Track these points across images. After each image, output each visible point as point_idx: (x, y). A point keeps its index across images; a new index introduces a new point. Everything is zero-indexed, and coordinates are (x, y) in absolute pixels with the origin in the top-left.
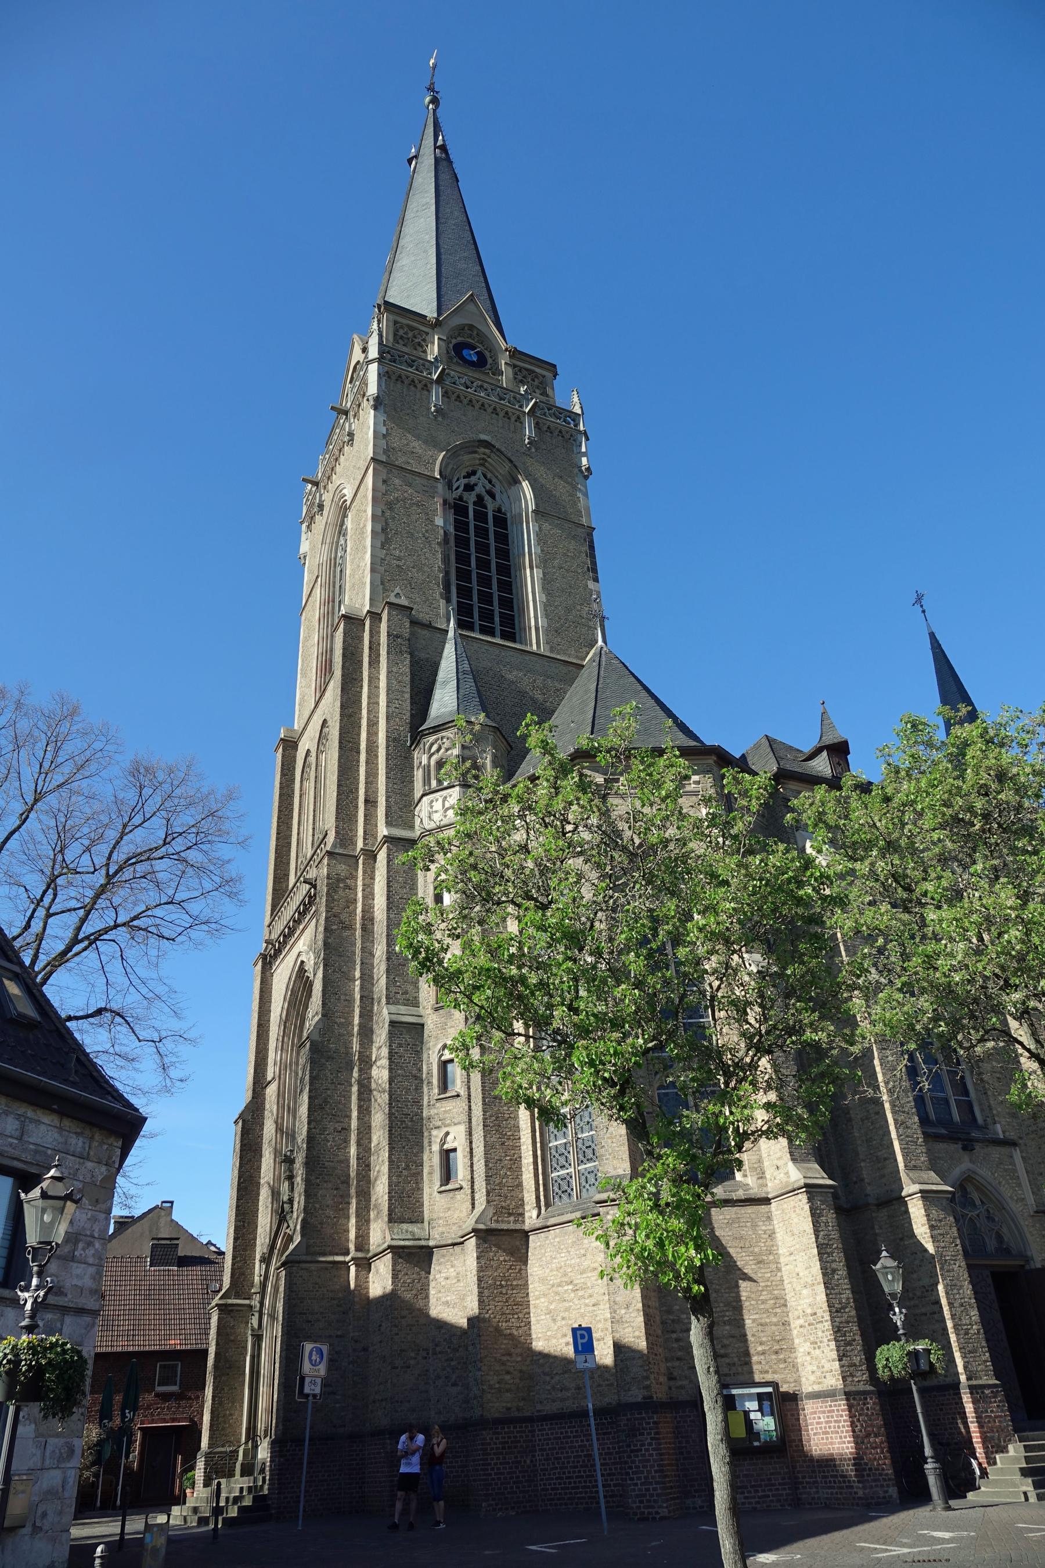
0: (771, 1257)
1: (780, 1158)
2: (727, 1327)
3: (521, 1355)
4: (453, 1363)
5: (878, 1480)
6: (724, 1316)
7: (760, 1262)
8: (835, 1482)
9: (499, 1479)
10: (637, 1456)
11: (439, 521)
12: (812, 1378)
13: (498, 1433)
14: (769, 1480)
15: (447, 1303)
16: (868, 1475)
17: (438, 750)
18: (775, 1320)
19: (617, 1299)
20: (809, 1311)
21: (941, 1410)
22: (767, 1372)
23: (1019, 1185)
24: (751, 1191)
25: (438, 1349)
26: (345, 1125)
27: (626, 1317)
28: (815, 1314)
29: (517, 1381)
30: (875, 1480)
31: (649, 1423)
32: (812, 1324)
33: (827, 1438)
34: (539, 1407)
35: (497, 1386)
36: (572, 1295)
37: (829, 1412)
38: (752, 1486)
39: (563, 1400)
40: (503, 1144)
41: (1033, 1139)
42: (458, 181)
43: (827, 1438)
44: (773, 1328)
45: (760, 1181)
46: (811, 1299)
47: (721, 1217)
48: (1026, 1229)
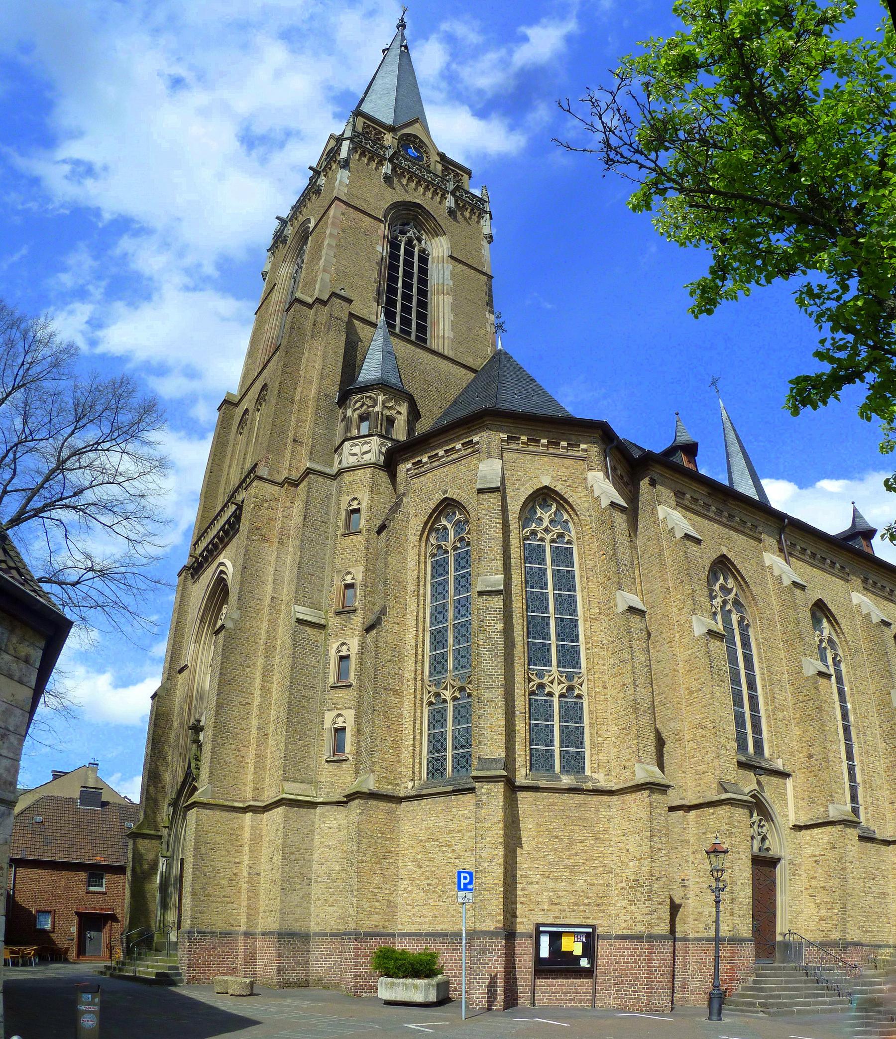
0: (607, 836)
1: (629, 760)
2: (564, 884)
3: (389, 889)
4: (330, 890)
6: (562, 875)
7: (597, 839)
8: (626, 995)
9: (366, 972)
10: (485, 967)
12: (624, 925)
13: (367, 942)
14: (576, 989)
15: (329, 847)
18: (602, 882)
19: (482, 854)
20: (632, 878)
22: (589, 918)
23: (786, 805)
24: (598, 784)
25: (319, 879)
26: (249, 701)
27: (489, 869)
28: (638, 880)
30: (659, 996)
32: (634, 887)
34: (400, 927)
36: (438, 849)
39: (421, 924)
40: (388, 727)
41: (804, 773)
44: (599, 887)
47: (571, 802)
48: (784, 837)
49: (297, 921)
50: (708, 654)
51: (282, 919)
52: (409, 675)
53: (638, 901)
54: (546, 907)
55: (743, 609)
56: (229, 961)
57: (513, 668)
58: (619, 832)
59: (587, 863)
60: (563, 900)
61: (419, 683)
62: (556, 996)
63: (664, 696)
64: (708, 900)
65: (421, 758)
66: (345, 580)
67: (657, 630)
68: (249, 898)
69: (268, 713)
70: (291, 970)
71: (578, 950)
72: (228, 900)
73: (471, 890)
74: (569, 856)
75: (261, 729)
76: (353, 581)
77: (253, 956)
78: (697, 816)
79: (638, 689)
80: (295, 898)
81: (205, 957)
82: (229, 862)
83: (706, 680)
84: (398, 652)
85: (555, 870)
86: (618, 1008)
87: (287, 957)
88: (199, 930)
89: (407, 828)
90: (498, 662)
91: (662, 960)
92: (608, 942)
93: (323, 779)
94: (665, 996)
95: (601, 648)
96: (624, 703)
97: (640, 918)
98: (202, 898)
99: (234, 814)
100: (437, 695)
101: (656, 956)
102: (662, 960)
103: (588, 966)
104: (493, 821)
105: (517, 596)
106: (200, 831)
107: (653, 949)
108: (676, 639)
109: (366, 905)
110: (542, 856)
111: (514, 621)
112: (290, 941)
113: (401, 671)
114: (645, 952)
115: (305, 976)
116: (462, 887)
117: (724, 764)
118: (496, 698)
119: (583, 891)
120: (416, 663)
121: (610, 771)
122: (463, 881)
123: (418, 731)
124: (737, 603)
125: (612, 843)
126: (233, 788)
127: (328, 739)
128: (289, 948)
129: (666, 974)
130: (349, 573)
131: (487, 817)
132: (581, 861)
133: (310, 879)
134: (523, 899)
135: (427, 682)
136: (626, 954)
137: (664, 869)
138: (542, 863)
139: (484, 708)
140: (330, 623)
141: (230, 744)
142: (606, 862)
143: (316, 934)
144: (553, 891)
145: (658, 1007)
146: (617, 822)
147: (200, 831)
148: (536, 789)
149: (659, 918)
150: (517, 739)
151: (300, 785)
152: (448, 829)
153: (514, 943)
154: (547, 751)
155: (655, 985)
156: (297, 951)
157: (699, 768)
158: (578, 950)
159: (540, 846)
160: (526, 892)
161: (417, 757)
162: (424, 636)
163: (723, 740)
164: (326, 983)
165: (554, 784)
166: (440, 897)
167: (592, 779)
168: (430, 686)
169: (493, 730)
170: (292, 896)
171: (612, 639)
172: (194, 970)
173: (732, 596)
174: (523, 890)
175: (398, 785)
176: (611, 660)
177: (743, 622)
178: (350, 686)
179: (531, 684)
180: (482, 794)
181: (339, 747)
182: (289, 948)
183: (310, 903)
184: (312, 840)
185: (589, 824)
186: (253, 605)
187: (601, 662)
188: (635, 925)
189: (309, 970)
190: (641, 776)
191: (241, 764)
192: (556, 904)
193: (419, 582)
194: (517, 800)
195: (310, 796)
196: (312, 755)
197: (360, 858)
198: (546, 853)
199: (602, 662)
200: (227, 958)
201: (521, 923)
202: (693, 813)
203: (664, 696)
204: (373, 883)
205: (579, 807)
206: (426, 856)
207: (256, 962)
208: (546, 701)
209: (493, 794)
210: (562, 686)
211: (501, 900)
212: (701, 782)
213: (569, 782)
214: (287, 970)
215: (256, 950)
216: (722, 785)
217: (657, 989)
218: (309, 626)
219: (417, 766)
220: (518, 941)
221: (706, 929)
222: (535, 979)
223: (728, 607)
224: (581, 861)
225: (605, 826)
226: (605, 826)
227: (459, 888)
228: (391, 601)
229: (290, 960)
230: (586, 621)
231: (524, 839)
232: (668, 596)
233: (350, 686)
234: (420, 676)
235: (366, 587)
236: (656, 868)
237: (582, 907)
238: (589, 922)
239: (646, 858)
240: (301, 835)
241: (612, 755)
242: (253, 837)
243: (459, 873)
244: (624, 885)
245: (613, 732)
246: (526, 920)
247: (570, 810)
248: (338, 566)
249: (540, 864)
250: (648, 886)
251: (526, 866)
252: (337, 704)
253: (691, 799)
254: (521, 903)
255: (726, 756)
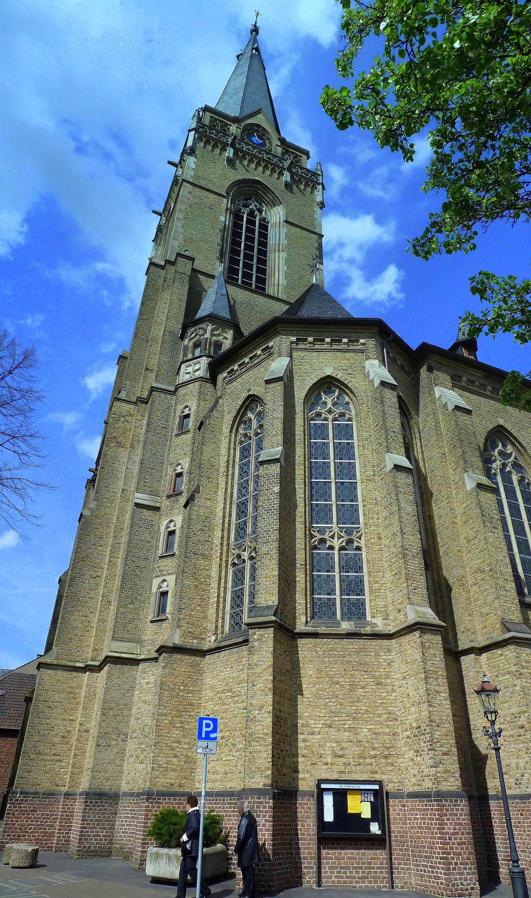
0: (389, 681)
1: (400, 604)
2: (347, 734)
3: (189, 744)
4: (142, 746)
5: (462, 874)
7: (378, 684)
11: (222, 219)
12: (413, 780)
13: (159, 803)
14: (370, 863)
15: (145, 702)
16: (454, 869)
17: (195, 336)
18: (387, 730)
19: (253, 702)
20: (415, 725)
21: (522, 814)
22: (376, 772)
24: (377, 629)
25: (134, 735)
26: (99, 574)
27: (258, 718)
28: (420, 727)
29: (183, 763)
31: (265, 807)
32: (417, 736)
33: (421, 833)
35: (165, 765)
36: (230, 700)
37: (424, 810)
38: (354, 868)
39: (214, 781)
42: (265, 69)
43: (421, 833)
44: (385, 737)
45: (385, 621)
46: (417, 715)
47: (351, 647)
49: (108, 779)
50: (479, 504)
51: (93, 778)
52: (217, 541)
53: (422, 751)
54: (329, 760)
55: (523, 470)
56: (48, 826)
57: (295, 526)
58: (400, 676)
59: (370, 710)
60: (347, 752)
61: (225, 547)
62: (346, 873)
63: (447, 546)
64: (513, 750)
65: (224, 613)
66: (176, 470)
67: (437, 490)
68: (76, 755)
69: (112, 584)
70: (94, 836)
71: (366, 812)
72: (57, 758)
73: (215, 739)
74: (351, 702)
75: (105, 597)
76: (182, 470)
77: (69, 819)
78: (488, 659)
79: (406, 536)
80: (109, 755)
81: (23, 821)
82: (64, 720)
83: (479, 527)
84: (209, 522)
85: (337, 719)
86: (420, 890)
87: (91, 820)
88: (23, 790)
89: (208, 680)
90: (274, 520)
91: (456, 824)
92: (400, 802)
93: (146, 638)
94: (468, 874)
95: (376, 504)
96: (395, 550)
97: (426, 771)
98: (32, 756)
99: (75, 674)
100: (239, 556)
101: (448, 819)
102: (456, 824)
103: (379, 832)
104: (264, 666)
105: (299, 466)
106: (40, 690)
107: (442, 810)
108: (453, 496)
109: (162, 760)
110: (323, 703)
111: (297, 486)
112: (96, 803)
113: (211, 539)
114: (435, 815)
115: (108, 844)
116: (203, 736)
117: (505, 604)
118: (272, 551)
119: (368, 742)
120: (223, 530)
121: (387, 616)
122: (204, 729)
123: (222, 589)
124: (516, 465)
125: (394, 688)
126: (77, 650)
127: (153, 602)
128: (95, 810)
129: (464, 843)
130: (179, 464)
131: (259, 663)
132: (364, 708)
133: (126, 735)
134: (305, 751)
135: (232, 546)
136: (418, 816)
137: (445, 714)
138: (323, 711)
139: (261, 560)
140: (163, 505)
141: (79, 611)
142: (390, 708)
143: (125, 794)
144: (336, 742)
145: (462, 890)
146: (397, 666)
147: (40, 690)
148: (315, 635)
149: (446, 771)
150: (298, 589)
151: (127, 644)
152: (239, 679)
153: (295, 804)
154: (329, 599)
155: (453, 858)
156: (103, 814)
157: (483, 610)
158: (366, 812)
159: (321, 693)
160: (307, 744)
161: (221, 613)
162: (231, 507)
163: (501, 582)
164: (127, 852)
165: (333, 630)
166: (231, 751)
167: (374, 625)
168: (234, 549)
169: (268, 579)
170: (106, 753)
171: (383, 496)
172: (8, 835)
173: (512, 459)
174: (304, 741)
175: (203, 639)
176: (384, 513)
177: (524, 481)
178: (174, 555)
179: (313, 540)
180: (255, 640)
181: (162, 608)
182: (95, 810)
183: (124, 760)
184: (132, 696)
185: (370, 669)
186: (108, 497)
187: (375, 516)
188: (423, 780)
189: (113, 836)
190: (412, 618)
191: (86, 629)
192: (340, 757)
193: (228, 464)
194: (297, 647)
195: (134, 654)
196: (141, 617)
197: (160, 711)
198: (328, 701)
199: (377, 516)
200: (46, 822)
201: (304, 779)
202: (484, 656)
203: (447, 546)
204: (172, 737)
205: (358, 652)
206: (222, 708)
207: (71, 826)
208: (328, 554)
209: (264, 639)
210: (342, 540)
211: (270, 752)
212: (487, 623)
213: (348, 627)
214: (89, 836)
215: (73, 812)
216: (504, 625)
217: (456, 864)
218: (146, 509)
219: (220, 621)
220: (299, 801)
221: (516, 784)
222: (319, 849)
223: (508, 469)
224: (364, 708)
225: (386, 670)
226: (386, 670)
227: (200, 737)
228: (204, 482)
229: (94, 824)
230: (362, 482)
231: (304, 686)
232: (444, 460)
233: (174, 555)
234: (226, 542)
235: (191, 474)
236: (435, 713)
237: (368, 760)
238: (378, 777)
239: (424, 702)
240: (121, 691)
241: (389, 599)
242: (87, 694)
243: (201, 720)
244: (408, 733)
245: (388, 578)
246: (308, 775)
247: (350, 655)
248: (172, 460)
249: (320, 712)
250: (428, 733)
251: (307, 714)
252: (163, 571)
253: (481, 641)
254: (302, 756)
255: (506, 597)
